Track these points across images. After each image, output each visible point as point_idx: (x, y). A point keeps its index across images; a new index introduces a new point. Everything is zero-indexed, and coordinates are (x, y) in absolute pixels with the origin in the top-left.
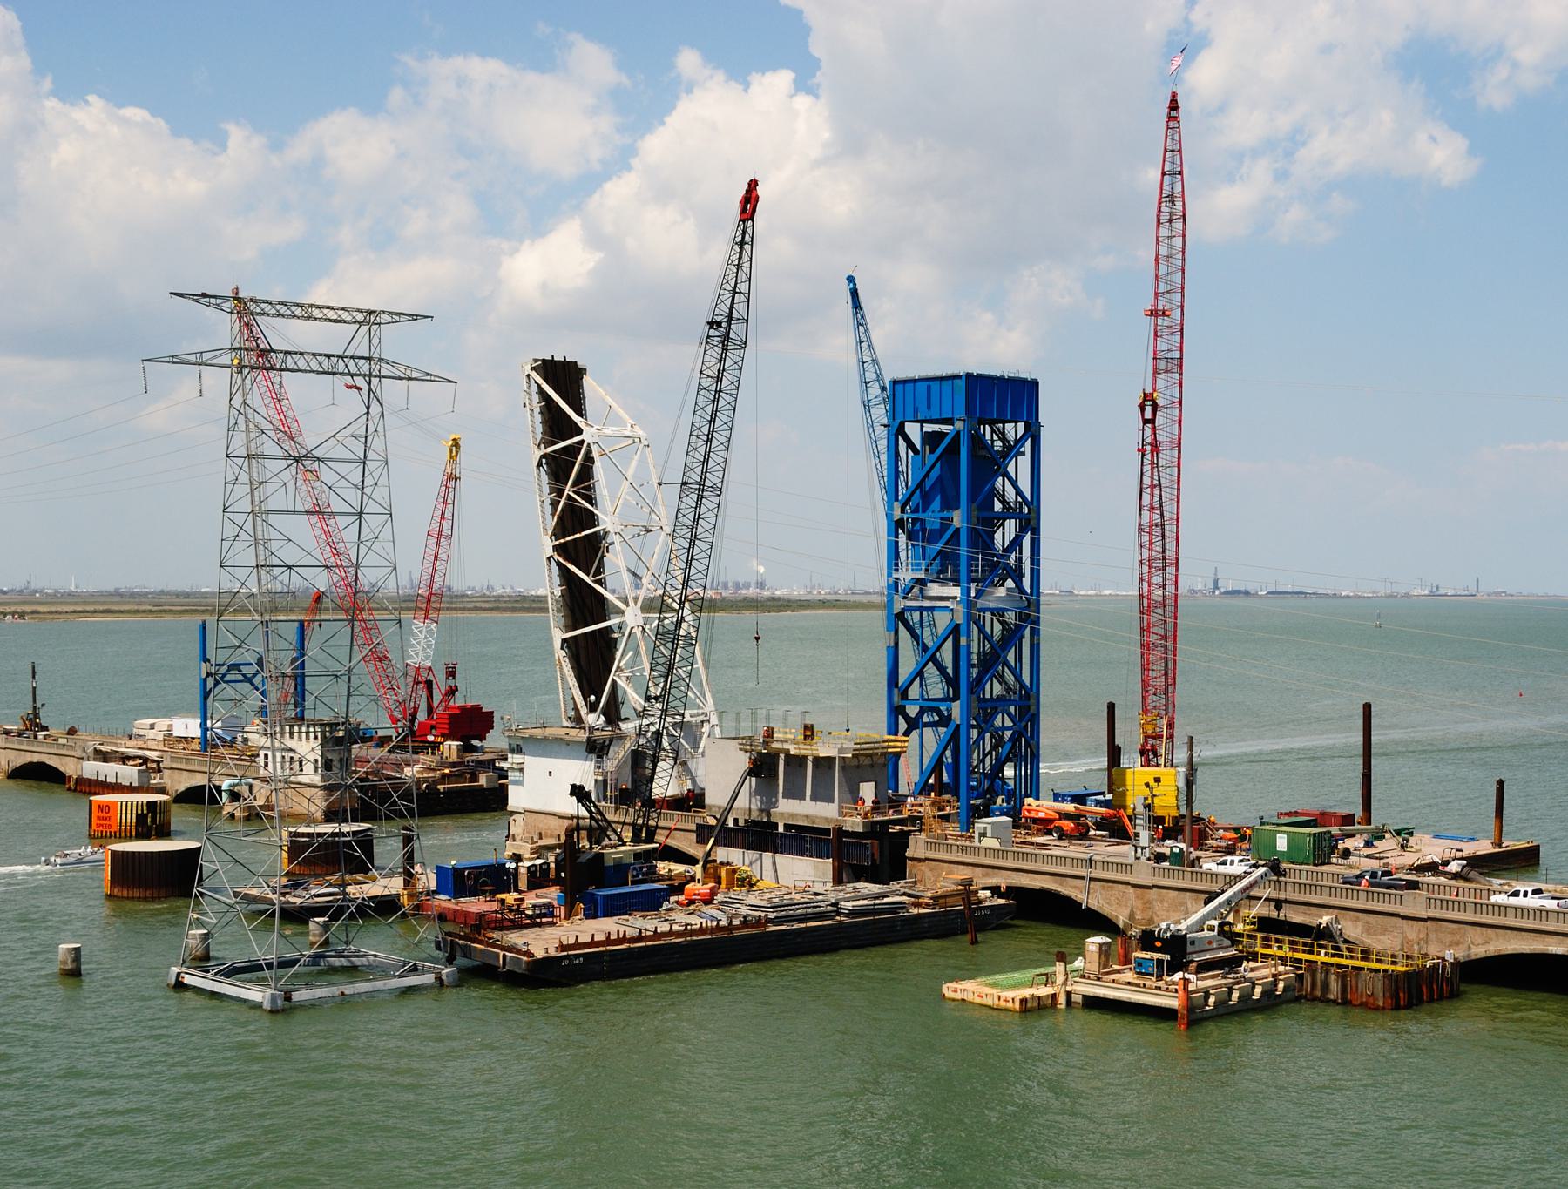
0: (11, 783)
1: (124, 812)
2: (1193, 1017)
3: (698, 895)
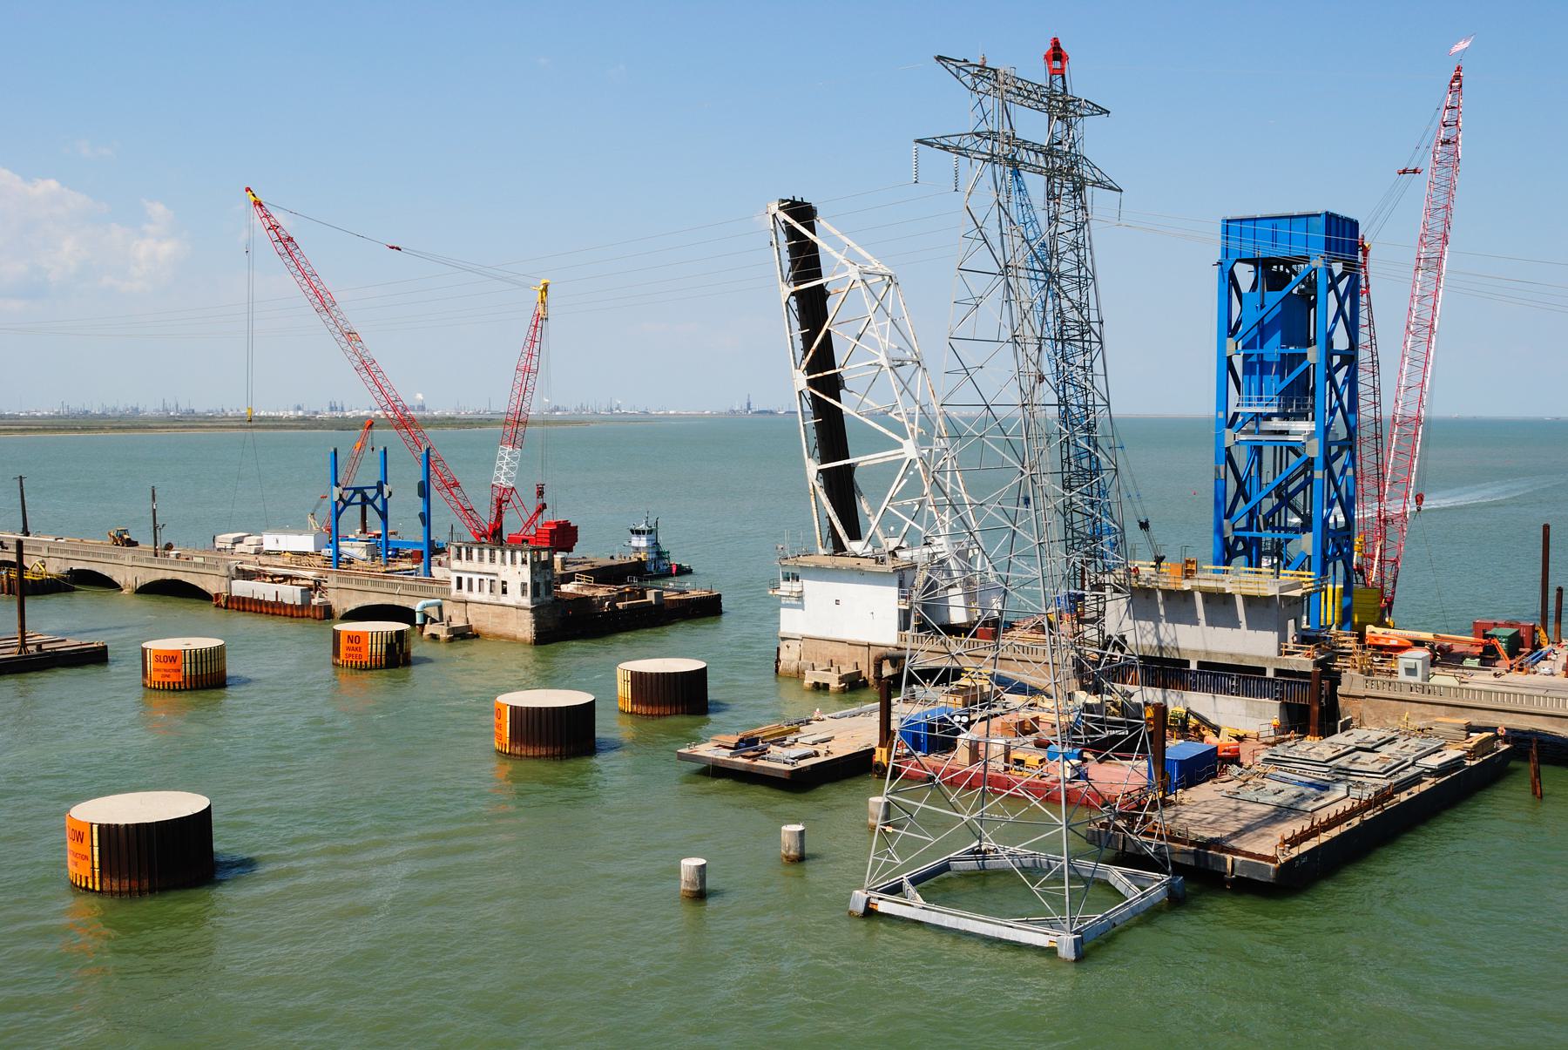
0: (136, 595)
1: (374, 642)
3: (1229, 751)
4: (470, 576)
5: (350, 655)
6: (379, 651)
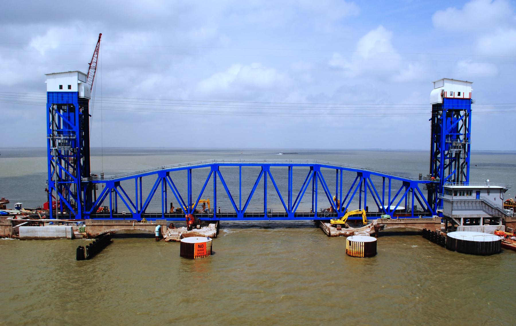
5: (199, 253)
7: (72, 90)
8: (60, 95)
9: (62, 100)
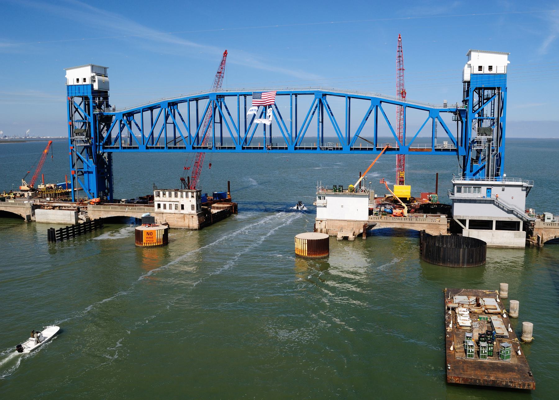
1: (158, 234)
2: (326, 232)
4: (165, 203)
5: (148, 240)
6: (160, 238)
7: (79, 83)
8: (77, 87)
9: (79, 92)
